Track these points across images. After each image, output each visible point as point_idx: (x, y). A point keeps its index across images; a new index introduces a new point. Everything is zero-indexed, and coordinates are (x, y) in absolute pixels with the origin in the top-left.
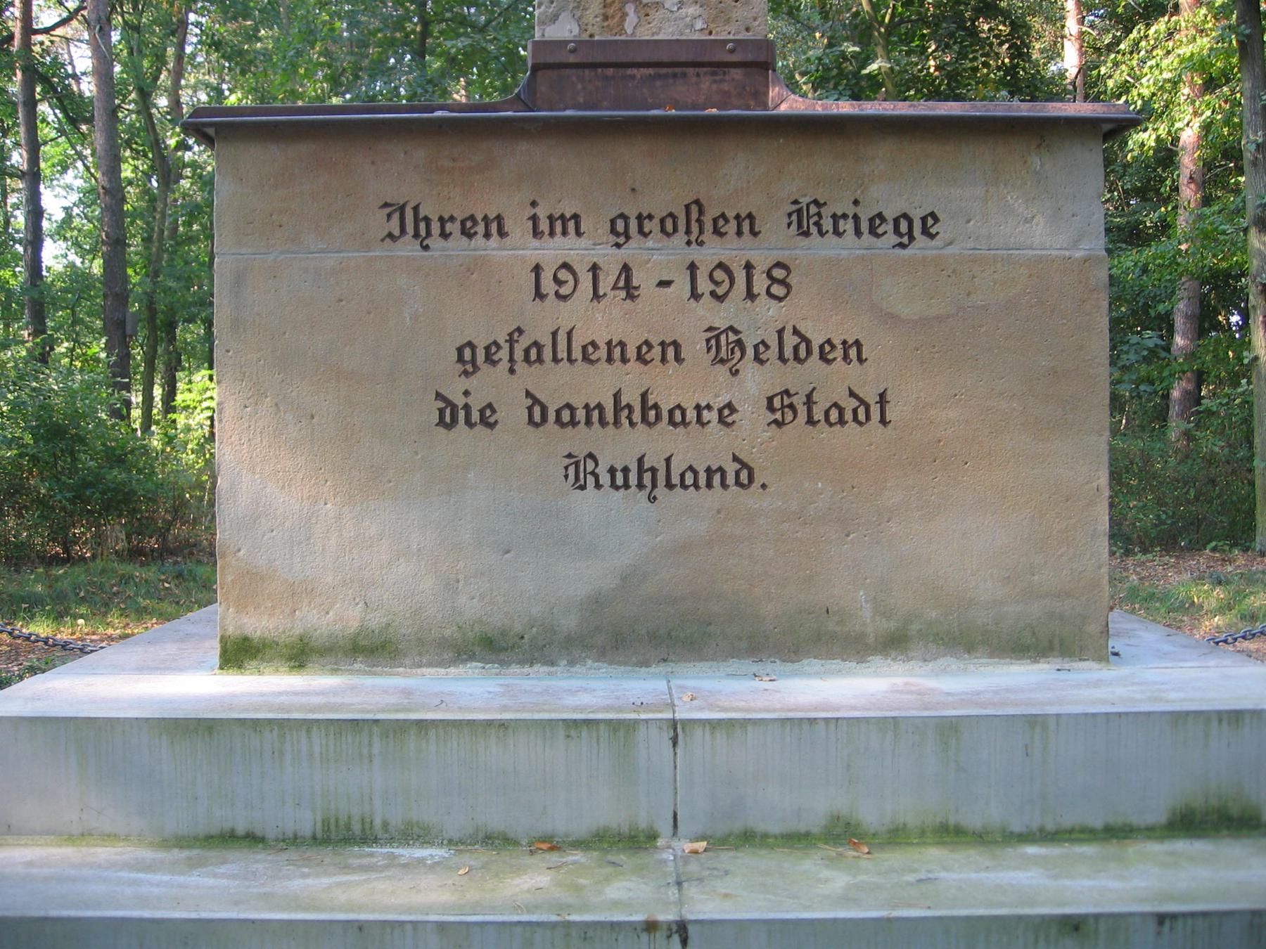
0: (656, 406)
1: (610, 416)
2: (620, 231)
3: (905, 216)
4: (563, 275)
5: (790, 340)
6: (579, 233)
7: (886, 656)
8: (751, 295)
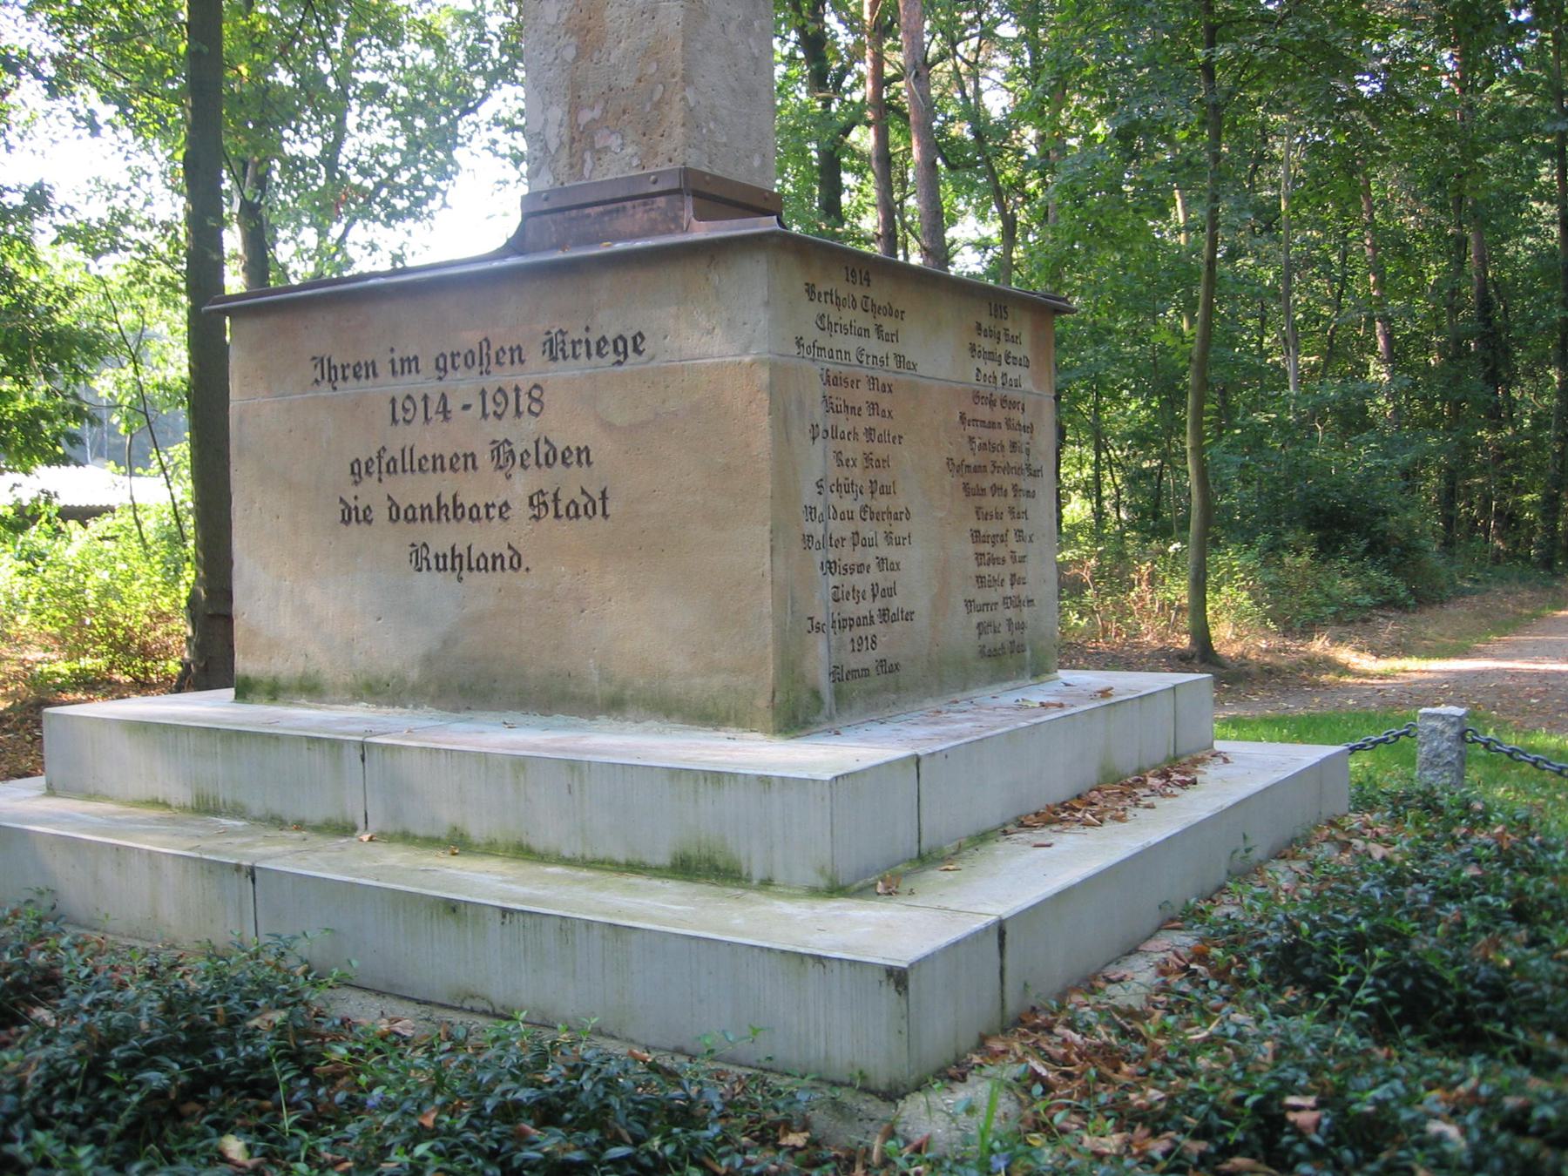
0: (462, 505)
1: (435, 515)
2: (443, 367)
3: (621, 337)
4: (409, 405)
5: (543, 448)
6: (418, 371)
7: (609, 716)
8: (518, 413)
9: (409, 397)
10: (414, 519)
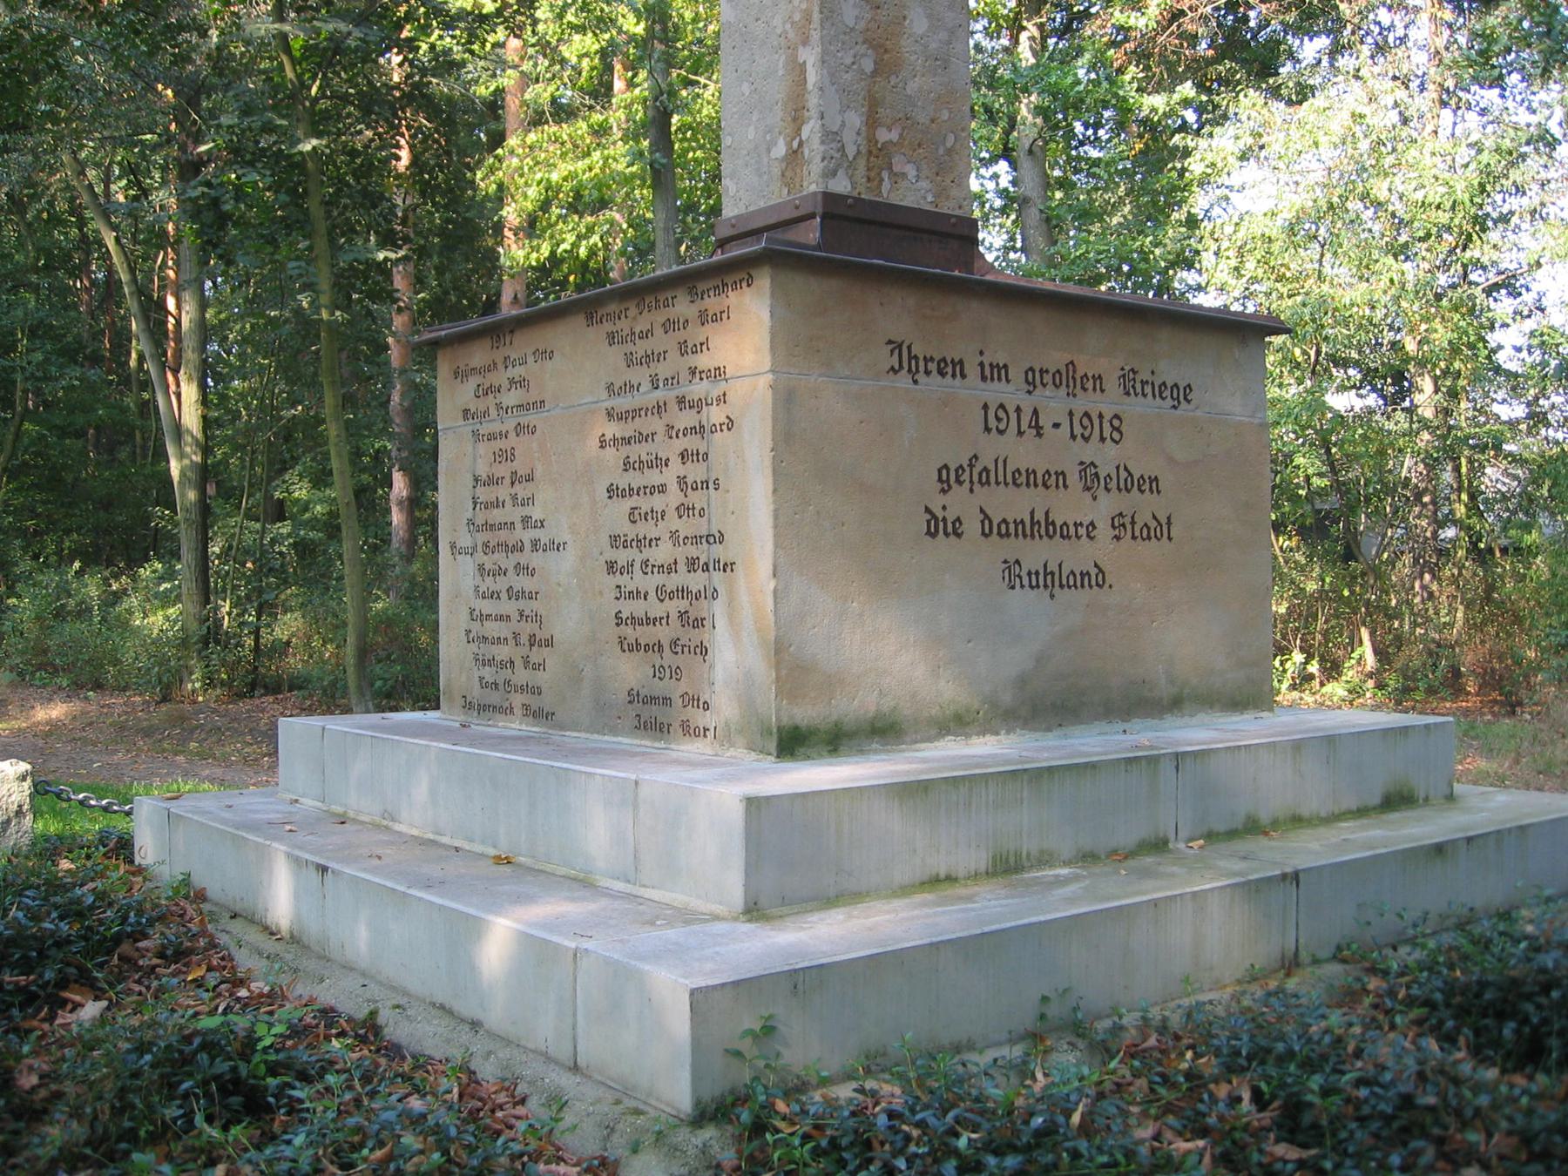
0: (1053, 523)
4: (1001, 414)
5: (1123, 474)
9: (1002, 406)
10: (1008, 535)
